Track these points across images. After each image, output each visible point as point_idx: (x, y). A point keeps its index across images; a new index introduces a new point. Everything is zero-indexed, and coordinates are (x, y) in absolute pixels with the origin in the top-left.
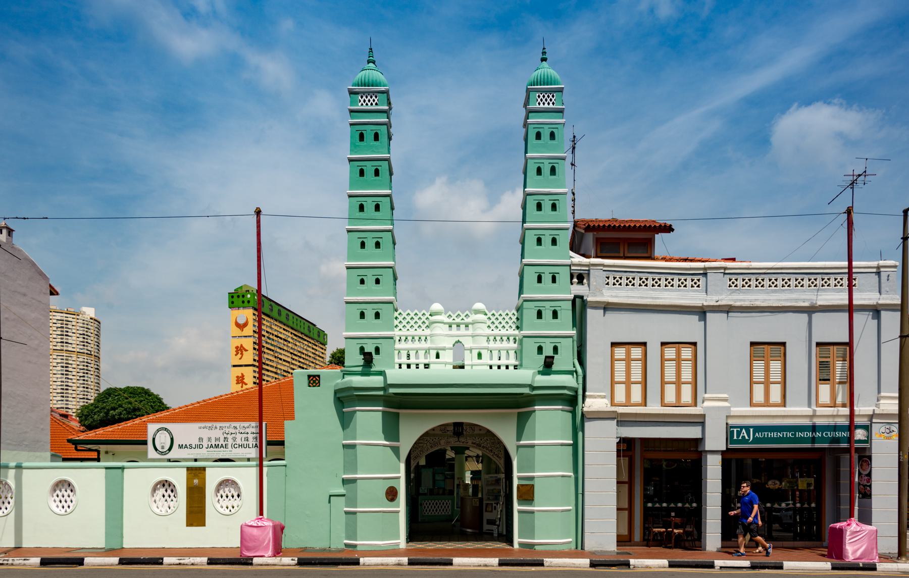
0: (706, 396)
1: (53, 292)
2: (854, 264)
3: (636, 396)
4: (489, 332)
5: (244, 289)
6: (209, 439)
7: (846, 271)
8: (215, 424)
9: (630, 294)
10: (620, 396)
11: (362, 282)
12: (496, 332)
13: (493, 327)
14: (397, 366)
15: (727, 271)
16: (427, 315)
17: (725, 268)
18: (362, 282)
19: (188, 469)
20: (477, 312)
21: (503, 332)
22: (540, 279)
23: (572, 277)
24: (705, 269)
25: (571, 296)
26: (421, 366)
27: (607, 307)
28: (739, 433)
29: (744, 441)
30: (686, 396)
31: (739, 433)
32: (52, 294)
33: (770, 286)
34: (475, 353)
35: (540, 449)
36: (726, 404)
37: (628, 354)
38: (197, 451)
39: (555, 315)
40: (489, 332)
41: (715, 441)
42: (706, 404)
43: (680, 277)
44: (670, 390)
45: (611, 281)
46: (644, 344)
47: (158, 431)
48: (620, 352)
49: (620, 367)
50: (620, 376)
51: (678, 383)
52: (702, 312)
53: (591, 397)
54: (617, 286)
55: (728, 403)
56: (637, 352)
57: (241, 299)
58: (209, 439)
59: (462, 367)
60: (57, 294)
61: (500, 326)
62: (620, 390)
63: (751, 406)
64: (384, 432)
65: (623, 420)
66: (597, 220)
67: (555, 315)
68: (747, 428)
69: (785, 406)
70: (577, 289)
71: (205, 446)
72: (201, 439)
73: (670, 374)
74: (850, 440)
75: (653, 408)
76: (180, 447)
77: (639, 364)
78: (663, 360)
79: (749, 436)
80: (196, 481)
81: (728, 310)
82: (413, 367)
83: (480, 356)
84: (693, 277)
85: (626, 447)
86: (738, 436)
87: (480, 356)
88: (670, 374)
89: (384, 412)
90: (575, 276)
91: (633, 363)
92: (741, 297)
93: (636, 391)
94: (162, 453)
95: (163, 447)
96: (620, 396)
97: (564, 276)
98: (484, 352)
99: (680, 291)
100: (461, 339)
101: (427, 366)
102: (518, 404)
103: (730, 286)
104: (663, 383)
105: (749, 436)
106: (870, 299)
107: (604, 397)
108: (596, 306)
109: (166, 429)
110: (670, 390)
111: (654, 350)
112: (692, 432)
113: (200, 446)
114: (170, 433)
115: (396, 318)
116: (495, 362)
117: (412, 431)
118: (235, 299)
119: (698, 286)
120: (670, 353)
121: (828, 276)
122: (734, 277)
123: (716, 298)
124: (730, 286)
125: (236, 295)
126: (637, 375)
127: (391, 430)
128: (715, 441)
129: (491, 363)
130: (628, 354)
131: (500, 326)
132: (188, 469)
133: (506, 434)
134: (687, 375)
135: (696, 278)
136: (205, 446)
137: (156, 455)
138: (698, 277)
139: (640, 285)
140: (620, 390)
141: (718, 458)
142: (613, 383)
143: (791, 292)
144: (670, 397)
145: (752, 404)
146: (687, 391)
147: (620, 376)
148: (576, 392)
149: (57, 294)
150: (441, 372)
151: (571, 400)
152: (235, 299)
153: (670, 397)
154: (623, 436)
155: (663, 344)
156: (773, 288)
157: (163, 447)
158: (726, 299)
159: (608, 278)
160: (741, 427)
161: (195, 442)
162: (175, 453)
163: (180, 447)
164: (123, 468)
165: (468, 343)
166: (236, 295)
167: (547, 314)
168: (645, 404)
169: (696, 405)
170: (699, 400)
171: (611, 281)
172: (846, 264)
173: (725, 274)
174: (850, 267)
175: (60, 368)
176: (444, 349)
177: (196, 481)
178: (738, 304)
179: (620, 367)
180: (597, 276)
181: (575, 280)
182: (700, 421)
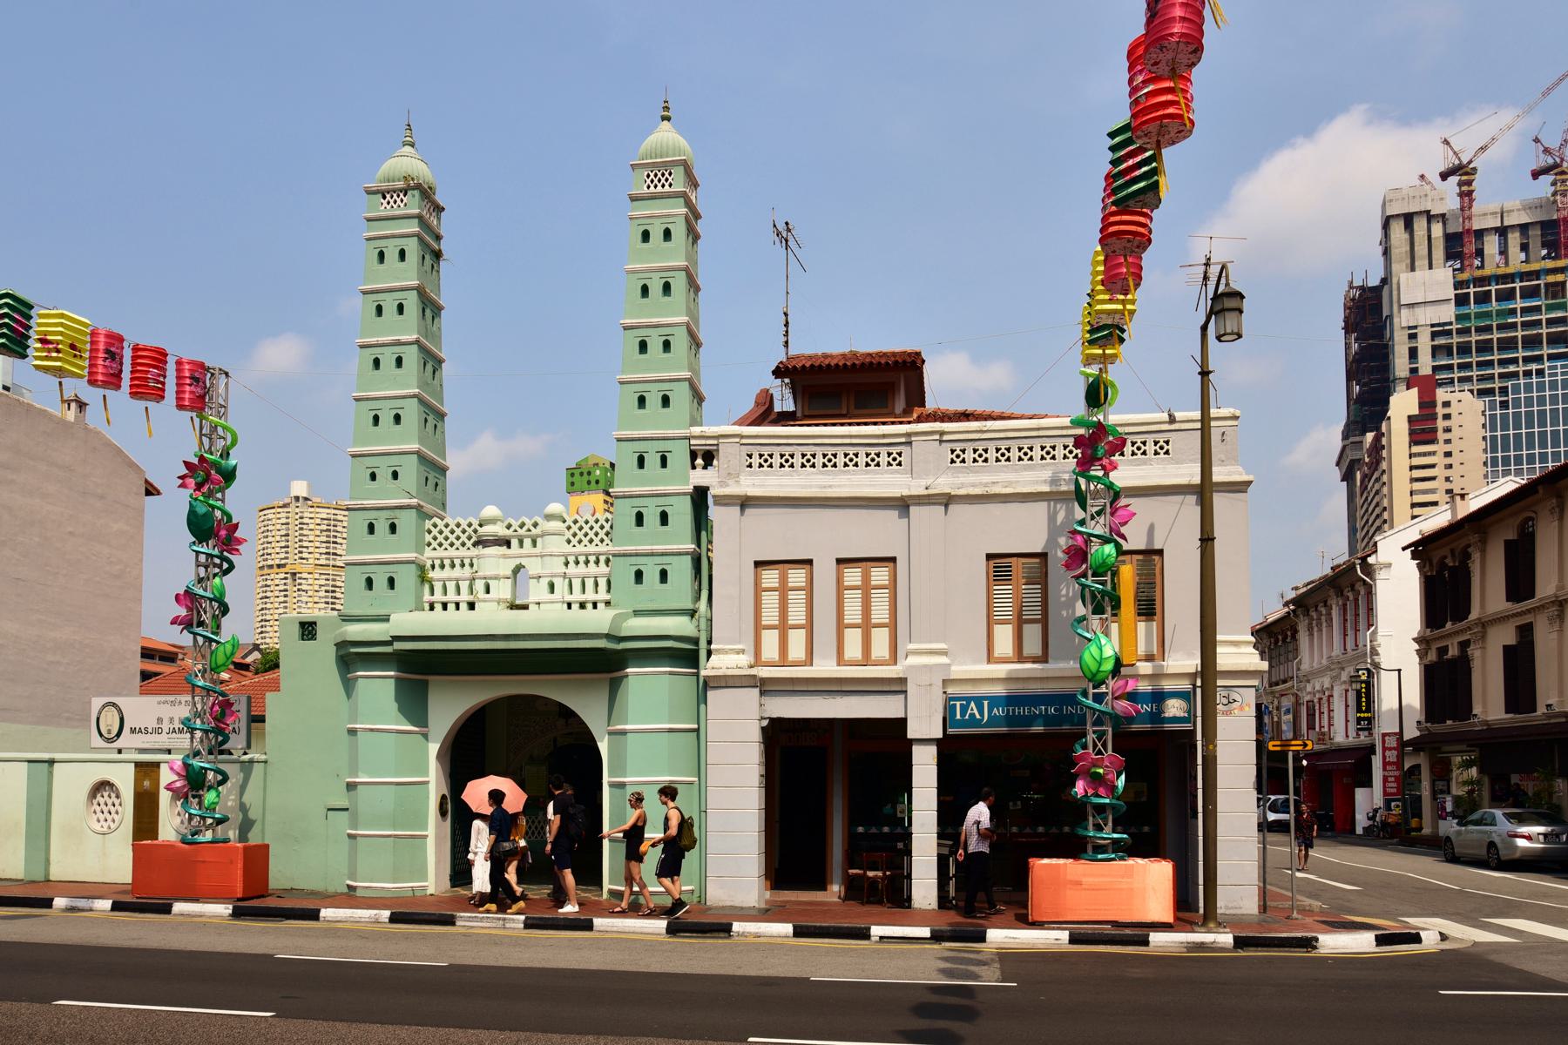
0: (911, 646)
1: (151, 491)
2: (1214, 412)
3: (797, 650)
4: (568, 549)
5: (591, 462)
6: (171, 720)
7: (1198, 425)
8: (179, 698)
9: (786, 480)
10: (770, 649)
11: (373, 477)
12: (580, 549)
13: (574, 541)
14: (427, 606)
15: (945, 438)
16: (476, 525)
17: (942, 433)
18: (373, 477)
19: (138, 765)
20: (549, 517)
21: (592, 549)
22: (641, 462)
23: (693, 455)
24: (908, 435)
25: (690, 488)
26: (464, 606)
27: (745, 503)
28: (964, 709)
29: (973, 721)
30: (880, 647)
31: (964, 709)
32: (148, 493)
33: (1020, 459)
34: (544, 582)
35: (637, 740)
36: (944, 660)
37: (783, 579)
38: (155, 737)
39: (664, 519)
40: (568, 549)
41: (925, 724)
42: (913, 660)
43: (869, 450)
44: (853, 639)
45: (756, 460)
46: (810, 562)
47: (104, 707)
48: (770, 577)
49: (770, 601)
50: (770, 615)
51: (867, 626)
52: (903, 505)
53: (719, 651)
54: (787, 469)
55: (944, 660)
56: (797, 577)
57: (586, 477)
58: (171, 720)
59: (525, 607)
60: (159, 493)
61: (457, 543)
62: (770, 640)
63: (989, 662)
64: (401, 710)
65: (767, 687)
66: (825, 356)
67: (664, 519)
68: (979, 701)
69: (1046, 661)
70: (700, 477)
71: (166, 730)
72: (160, 720)
73: (853, 612)
74: (1157, 717)
75: (824, 667)
76: (133, 731)
77: (802, 595)
78: (840, 588)
79: (982, 714)
80: (146, 783)
81: (947, 500)
82: (451, 607)
83: (552, 587)
84: (891, 449)
85: (778, 735)
86: (963, 714)
87: (552, 587)
88: (853, 612)
89: (397, 679)
90: (700, 455)
91: (792, 595)
92: (972, 478)
93: (797, 640)
94: (109, 740)
95: (109, 732)
96: (770, 649)
97: (679, 456)
98: (558, 582)
99: (867, 473)
100: (524, 561)
101: (472, 606)
102: (604, 663)
103: (953, 461)
104: (841, 627)
105: (982, 714)
106: (974, 485)
107: (743, 651)
108: (723, 501)
109: (114, 705)
110: (853, 639)
111: (825, 570)
112: (1416, 449)
113: (158, 731)
114: (120, 711)
115: (430, 532)
116: (577, 596)
117: (449, 707)
118: (577, 478)
119: (900, 464)
120: (853, 576)
121: (876, 450)
122: (958, 447)
123: (924, 483)
124: (953, 461)
125: (577, 472)
126: (797, 614)
127: (413, 702)
128: (925, 724)
129: (569, 598)
130: (866, 578)
131: (585, 541)
132: (138, 765)
133: (590, 709)
134: (880, 612)
135: (895, 450)
136: (166, 730)
137: (98, 742)
138: (898, 449)
139: (803, 466)
140: (770, 640)
141: (932, 750)
142: (758, 627)
143: (970, 470)
144: (853, 649)
145: (990, 658)
146: (880, 639)
147: (770, 615)
148: (696, 641)
149: (159, 493)
150: (490, 619)
151: (686, 655)
152: (577, 478)
153: (853, 649)
154: (774, 716)
155: (758, 564)
156: (1026, 462)
157: (109, 732)
158: (945, 483)
159: (750, 456)
160: (969, 699)
161: (152, 724)
162: (126, 740)
163: (133, 731)
164: (52, 762)
165: (533, 567)
166: (577, 472)
167: (651, 518)
168: (809, 661)
169: (895, 663)
170: (900, 653)
171: (756, 460)
172: (1197, 415)
173: (941, 441)
174: (1205, 419)
175: (323, 594)
176: (496, 578)
177: (146, 783)
178: (962, 492)
179: (770, 601)
180: (729, 455)
181: (699, 461)
182: (897, 687)
